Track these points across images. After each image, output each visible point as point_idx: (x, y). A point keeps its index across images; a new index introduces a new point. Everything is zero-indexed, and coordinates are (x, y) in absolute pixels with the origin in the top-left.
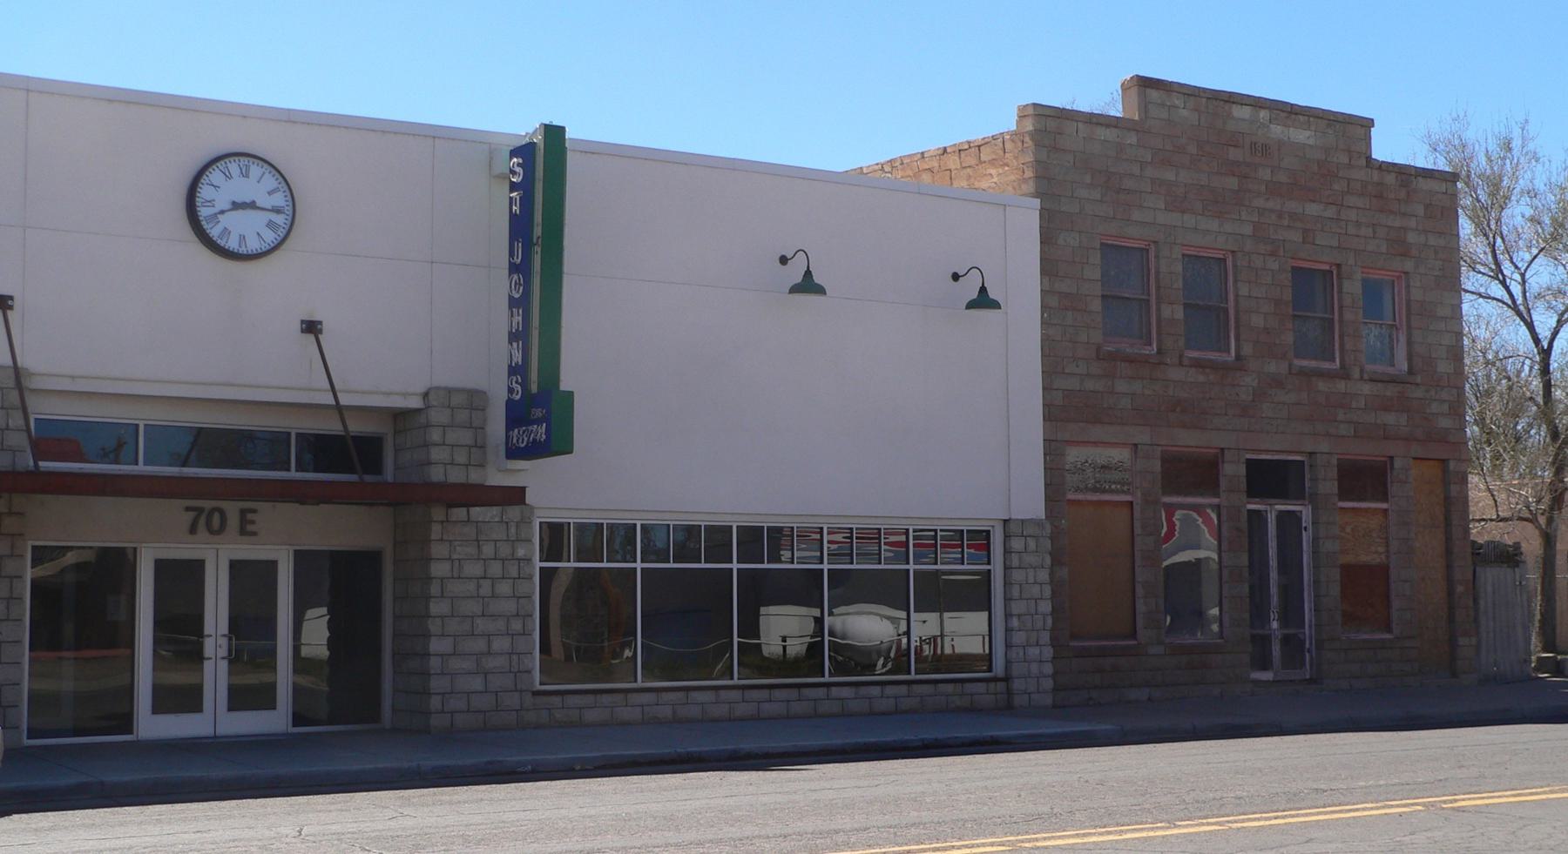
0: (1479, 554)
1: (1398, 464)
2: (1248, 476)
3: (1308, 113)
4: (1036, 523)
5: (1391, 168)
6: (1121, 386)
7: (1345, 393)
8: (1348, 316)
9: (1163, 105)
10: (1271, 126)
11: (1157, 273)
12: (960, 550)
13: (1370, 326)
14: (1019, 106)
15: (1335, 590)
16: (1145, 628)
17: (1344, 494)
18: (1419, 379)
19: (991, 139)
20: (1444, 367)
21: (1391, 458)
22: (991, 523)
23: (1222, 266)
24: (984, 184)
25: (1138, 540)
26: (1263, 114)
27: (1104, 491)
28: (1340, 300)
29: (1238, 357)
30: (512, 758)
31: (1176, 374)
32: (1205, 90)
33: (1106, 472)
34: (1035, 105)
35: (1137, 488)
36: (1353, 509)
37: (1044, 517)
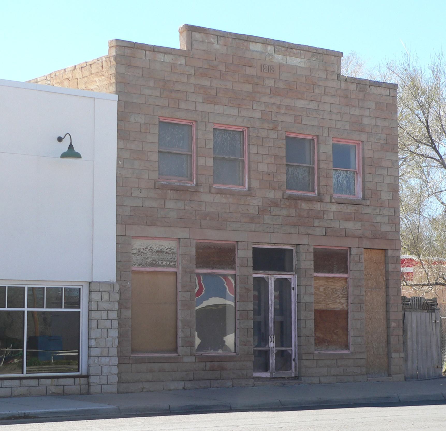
0: (408, 304)
1: (354, 251)
2: (254, 258)
3: (299, 48)
5: (353, 81)
6: (170, 205)
8: (322, 166)
9: (203, 42)
11: (197, 139)
12: (417, 308)
13: (339, 172)
14: (109, 41)
15: (311, 324)
16: (183, 346)
17: (317, 269)
18: (368, 203)
19: (96, 60)
20: (385, 196)
21: (350, 248)
22: (81, 284)
24: (92, 87)
25: (179, 294)
26: (270, 49)
27: (158, 266)
28: (318, 156)
29: (249, 189)
31: (207, 198)
32: (231, 34)
33: (160, 254)
34: (117, 40)
35: (179, 264)
36: (325, 277)
37: (115, 281)
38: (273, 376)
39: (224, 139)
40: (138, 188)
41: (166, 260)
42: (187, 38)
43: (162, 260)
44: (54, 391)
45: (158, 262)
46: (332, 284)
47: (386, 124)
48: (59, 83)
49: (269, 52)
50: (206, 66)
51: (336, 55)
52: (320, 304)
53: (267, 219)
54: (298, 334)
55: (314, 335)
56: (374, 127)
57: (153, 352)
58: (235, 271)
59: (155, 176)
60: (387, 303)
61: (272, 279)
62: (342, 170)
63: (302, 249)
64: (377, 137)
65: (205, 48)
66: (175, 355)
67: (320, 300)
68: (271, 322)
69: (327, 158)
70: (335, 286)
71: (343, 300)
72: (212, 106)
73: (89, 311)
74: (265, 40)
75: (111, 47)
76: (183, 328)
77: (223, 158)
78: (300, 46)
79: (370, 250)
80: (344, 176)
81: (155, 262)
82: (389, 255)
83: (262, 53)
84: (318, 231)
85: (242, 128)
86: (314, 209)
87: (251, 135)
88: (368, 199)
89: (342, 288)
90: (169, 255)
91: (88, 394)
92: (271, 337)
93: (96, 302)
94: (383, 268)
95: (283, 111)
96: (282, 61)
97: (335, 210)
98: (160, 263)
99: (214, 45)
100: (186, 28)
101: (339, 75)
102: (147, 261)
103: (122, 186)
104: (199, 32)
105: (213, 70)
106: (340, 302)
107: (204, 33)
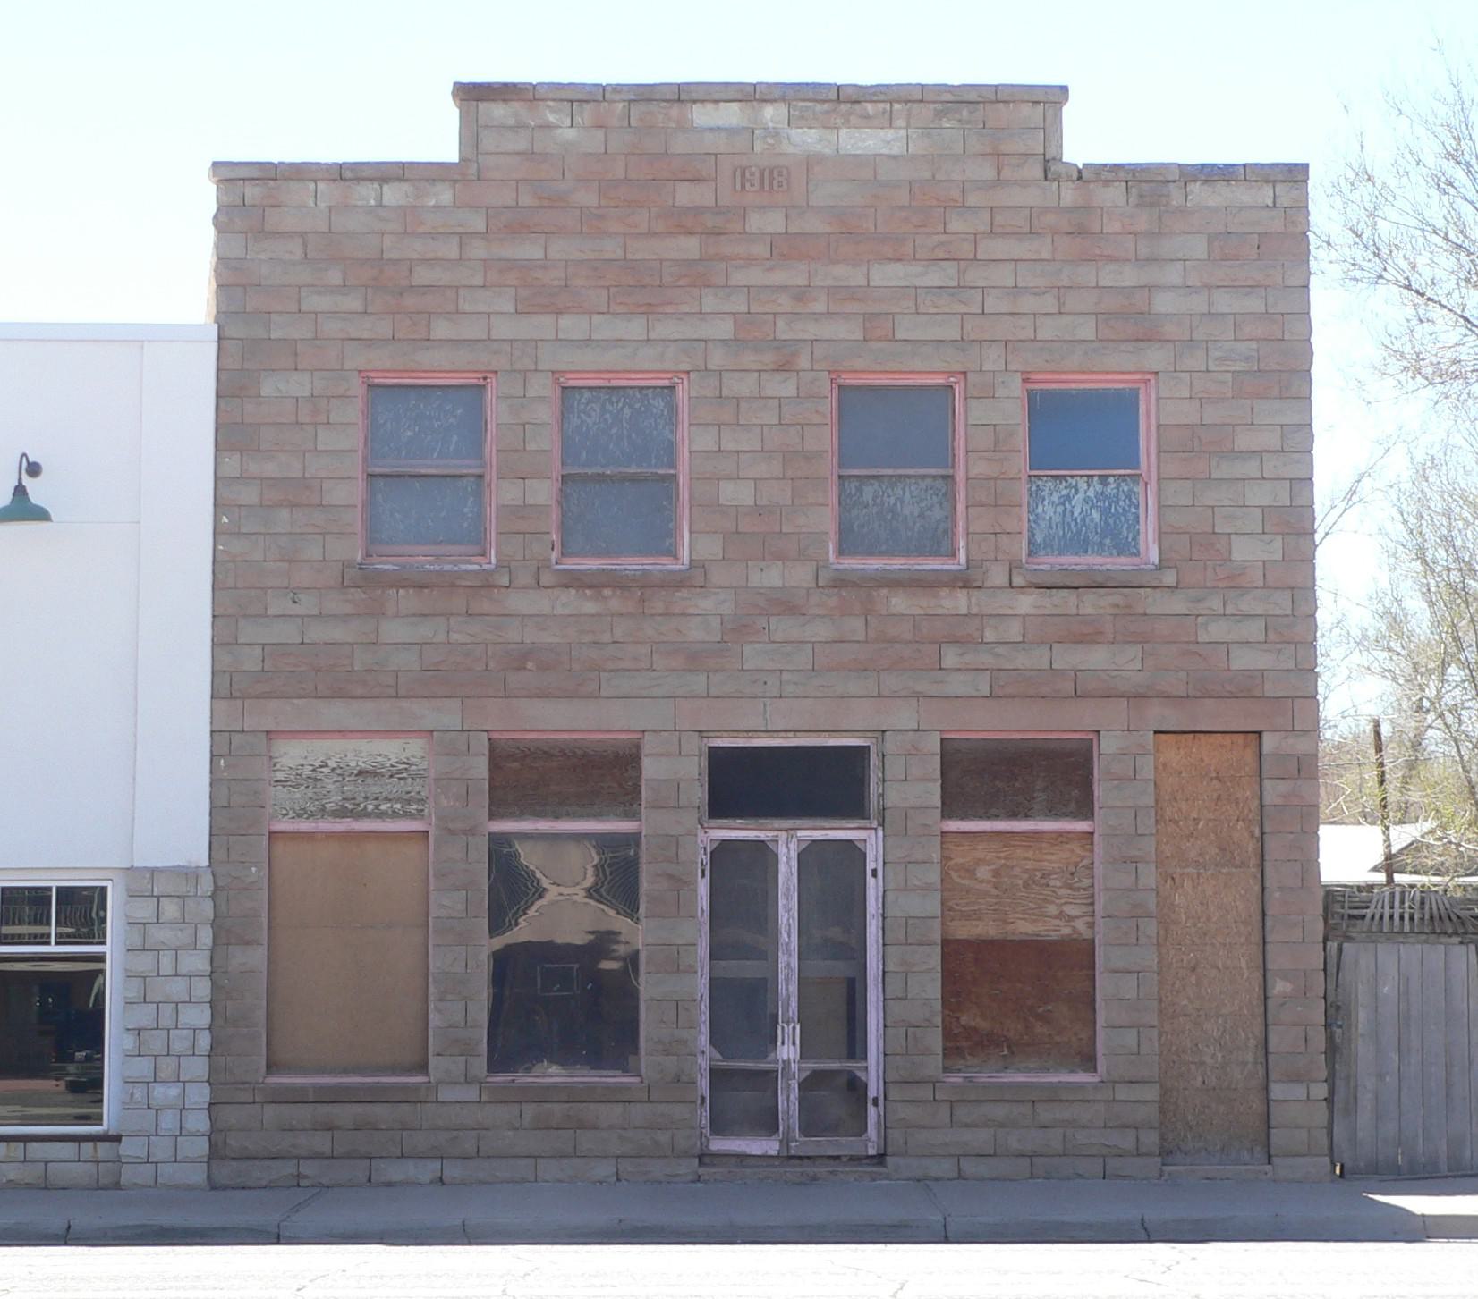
0: (1363, 917)
1: (1109, 745)
4: (187, 874)
5: (1106, 176)
9: (519, 127)
10: (793, 132)
12: (1407, 928)
13: (1073, 482)
15: (930, 987)
16: (439, 1055)
18: (1170, 578)
25: (433, 896)
26: (771, 114)
27: (365, 814)
30: (489, 1241)
31: (520, 602)
32: (618, 88)
33: (370, 781)
37: (206, 863)
41: (390, 797)
43: (377, 799)
44: (12, 1176)
45: (362, 805)
46: (1030, 854)
47: (1255, 304)
49: (771, 125)
50: (526, 200)
52: (974, 923)
53: (755, 655)
57: (345, 1071)
58: (637, 823)
62: (1082, 476)
65: (522, 145)
66: (420, 1079)
68: (787, 980)
69: (997, 442)
71: (1072, 906)
76: (441, 1000)
77: (601, 478)
79: (1191, 736)
80: (1091, 494)
81: (354, 804)
84: (958, 685)
85: (669, 376)
86: (946, 612)
90: (402, 782)
92: (783, 1028)
93: (141, 926)
95: (820, 307)
96: (819, 147)
97: (1033, 611)
98: (370, 807)
99: (560, 131)
105: (557, 207)
107: (523, 100)
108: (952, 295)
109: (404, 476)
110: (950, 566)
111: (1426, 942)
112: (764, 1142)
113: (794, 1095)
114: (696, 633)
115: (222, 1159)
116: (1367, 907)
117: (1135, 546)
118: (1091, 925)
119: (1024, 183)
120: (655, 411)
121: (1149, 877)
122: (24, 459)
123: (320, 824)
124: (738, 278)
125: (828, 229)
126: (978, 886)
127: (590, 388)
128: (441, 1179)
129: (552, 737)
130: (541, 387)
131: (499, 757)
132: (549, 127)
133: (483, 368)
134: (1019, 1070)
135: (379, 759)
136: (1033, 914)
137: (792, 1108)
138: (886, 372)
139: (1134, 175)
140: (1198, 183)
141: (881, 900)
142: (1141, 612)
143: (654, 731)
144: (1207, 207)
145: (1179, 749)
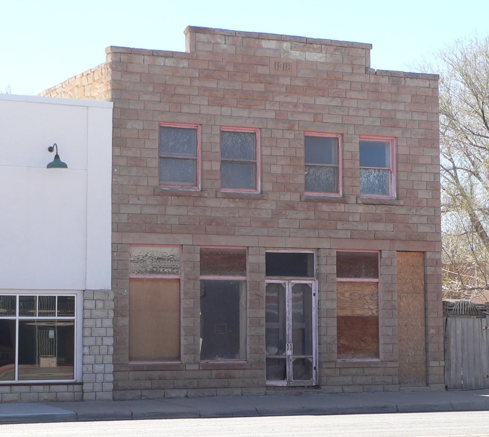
0: (452, 310)
1: (384, 254)
3: (319, 43)
4: (105, 292)
5: (384, 74)
6: (171, 211)
7: (344, 212)
8: (347, 165)
9: (209, 43)
10: (292, 52)
12: (463, 313)
13: (370, 170)
15: (333, 331)
16: (185, 354)
17: (340, 274)
18: (402, 203)
20: (423, 195)
21: (381, 251)
23: (195, 133)
24: (95, 94)
25: (182, 301)
26: (286, 45)
27: (160, 273)
31: (211, 203)
32: (240, 32)
33: (161, 261)
34: (111, 47)
36: (351, 282)
37: (111, 289)
38: (290, 385)
39: (234, 141)
40: (135, 195)
42: (190, 40)
43: (163, 268)
44: (46, 397)
46: (360, 289)
47: (424, 118)
48: (71, 90)
49: (285, 49)
50: (212, 68)
51: (363, 48)
52: (344, 311)
53: (282, 223)
54: (319, 341)
55: (336, 342)
56: (410, 122)
57: (154, 360)
59: (155, 182)
60: (426, 309)
61: (290, 285)
62: (373, 169)
63: (322, 252)
64: (413, 133)
65: (211, 49)
67: (345, 306)
68: (289, 329)
69: (352, 157)
70: (364, 291)
71: (372, 306)
72: (219, 108)
73: (83, 319)
74: (280, 37)
75: (108, 54)
76: (186, 336)
77: (233, 162)
78: (320, 40)
79: (405, 252)
80: (375, 175)
82: (427, 258)
83: (275, 50)
84: (341, 234)
85: (254, 129)
86: (337, 211)
87: (263, 136)
88: (403, 199)
89: (372, 294)
90: (171, 262)
91: (82, 401)
92: (288, 345)
94: (421, 271)
95: (301, 110)
96: (299, 58)
98: (161, 270)
100: (189, 30)
101: (367, 69)
102: (146, 268)
103: (119, 194)
104: (204, 33)
105: (220, 71)
106: (369, 308)
107: (210, 34)
108: (340, 109)
109: (169, 158)
110: (337, 196)
111: (468, 317)
112: (282, 382)
113: (291, 367)
114: (265, 215)
115: (116, 390)
116: (453, 307)
117: (388, 192)
118: (377, 312)
119: (360, 74)
120: (248, 140)
121: (395, 298)
122: (55, 145)
123: (146, 276)
124: (277, 99)
125: (303, 84)
126: (346, 299)
127: (229, 132)
128: (187, 396)
129: (219, 248)
130: (216, 131)
131: (203, 254)
132: (217, 43)
133: (198, 123)
134: (357, 358)
135: (164, 254)
136: (361, 308)
137: (290, 370)
138: (320, 132)
139: (391, 74)
140: (409, 79)
141: (317, 303)
142: (393, 213)
143: (252, 247)
144: (411, 86)
145: (402, 256)
